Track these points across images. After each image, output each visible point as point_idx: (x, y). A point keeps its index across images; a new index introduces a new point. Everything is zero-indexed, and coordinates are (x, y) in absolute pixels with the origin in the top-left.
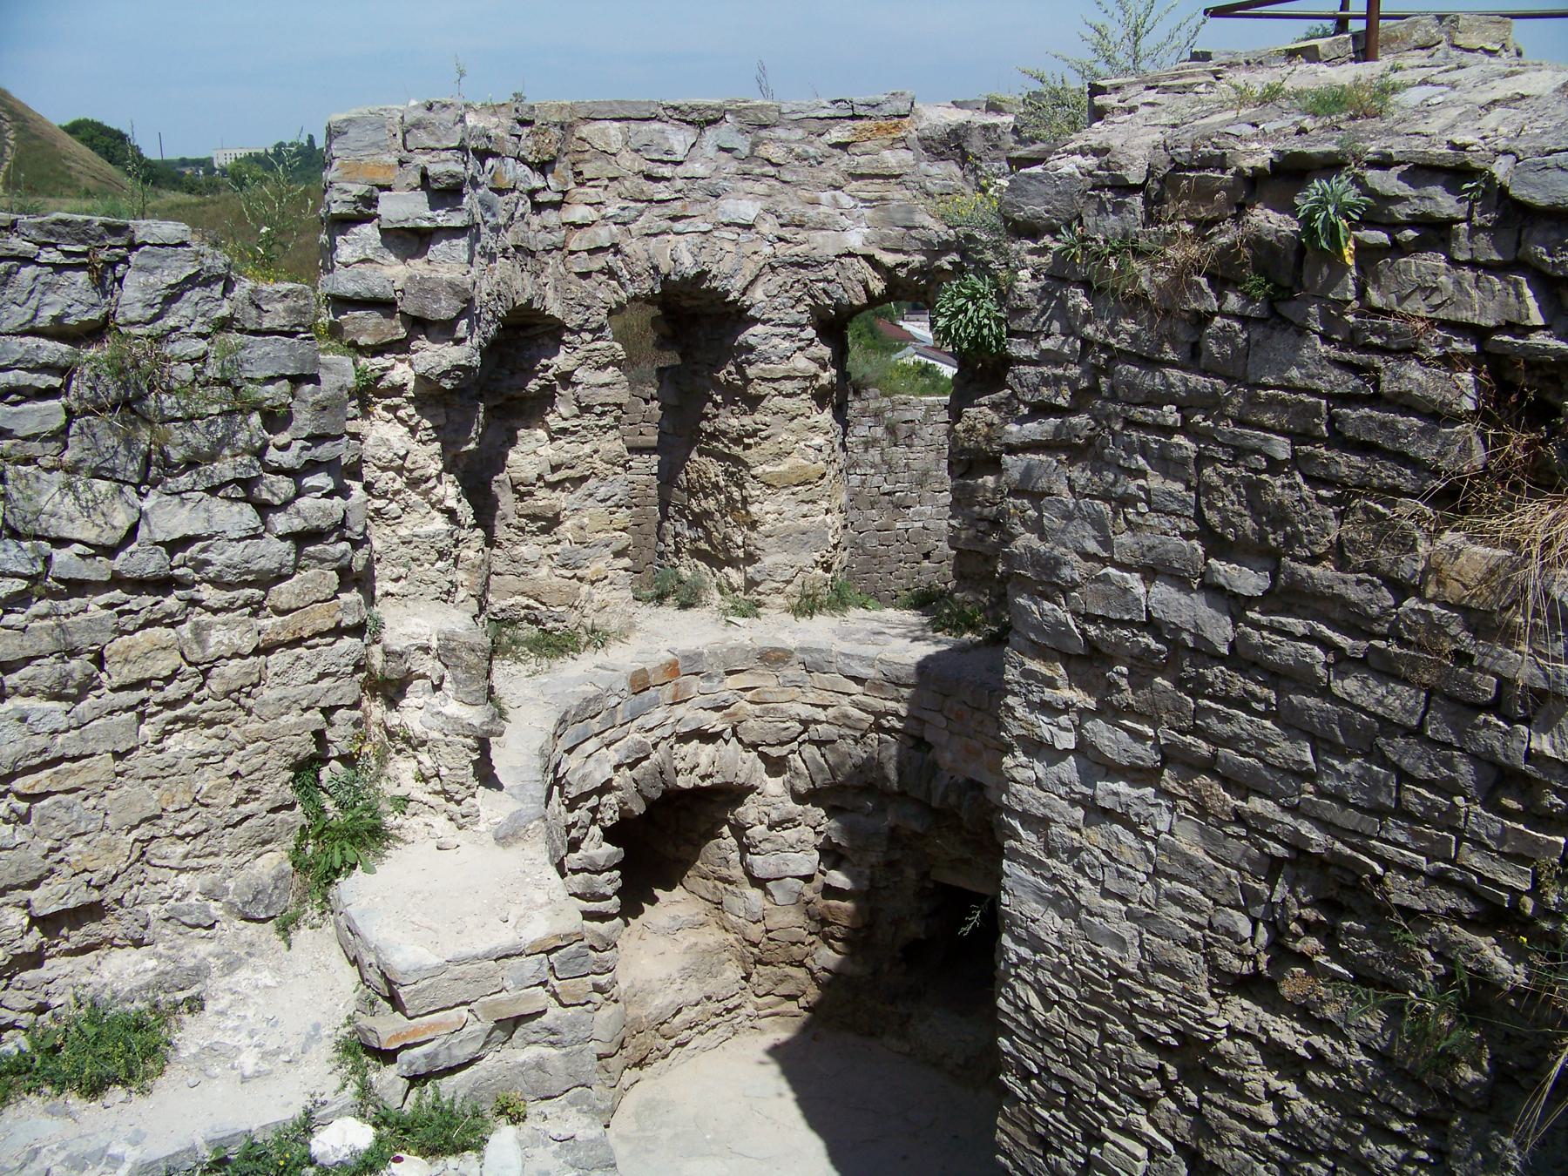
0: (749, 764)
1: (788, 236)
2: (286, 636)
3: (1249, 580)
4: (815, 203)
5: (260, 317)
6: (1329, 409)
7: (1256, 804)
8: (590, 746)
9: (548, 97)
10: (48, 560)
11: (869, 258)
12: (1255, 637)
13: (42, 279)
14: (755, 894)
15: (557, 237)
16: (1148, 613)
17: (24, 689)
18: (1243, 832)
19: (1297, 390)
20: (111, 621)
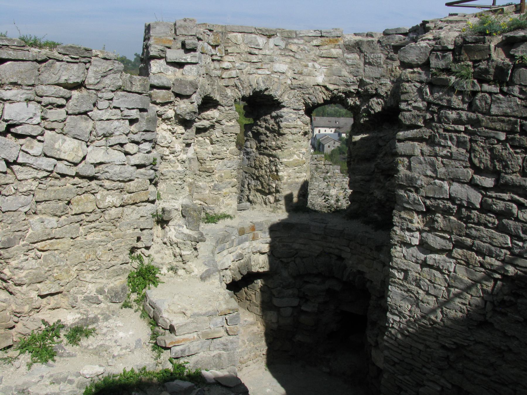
1: (297, 78)
2: (131, 202)
3: (488, 182)
5: (132, 86)
6: (520, 122)
9: (216, 22)
11: (325, 87)
12: (490, 201)
13: (63, 66)
15: (218, 73)
16: (450, 194)
17: (43, 212)
18: (483, 270)
19: (508, 116)
20: (74, 190)
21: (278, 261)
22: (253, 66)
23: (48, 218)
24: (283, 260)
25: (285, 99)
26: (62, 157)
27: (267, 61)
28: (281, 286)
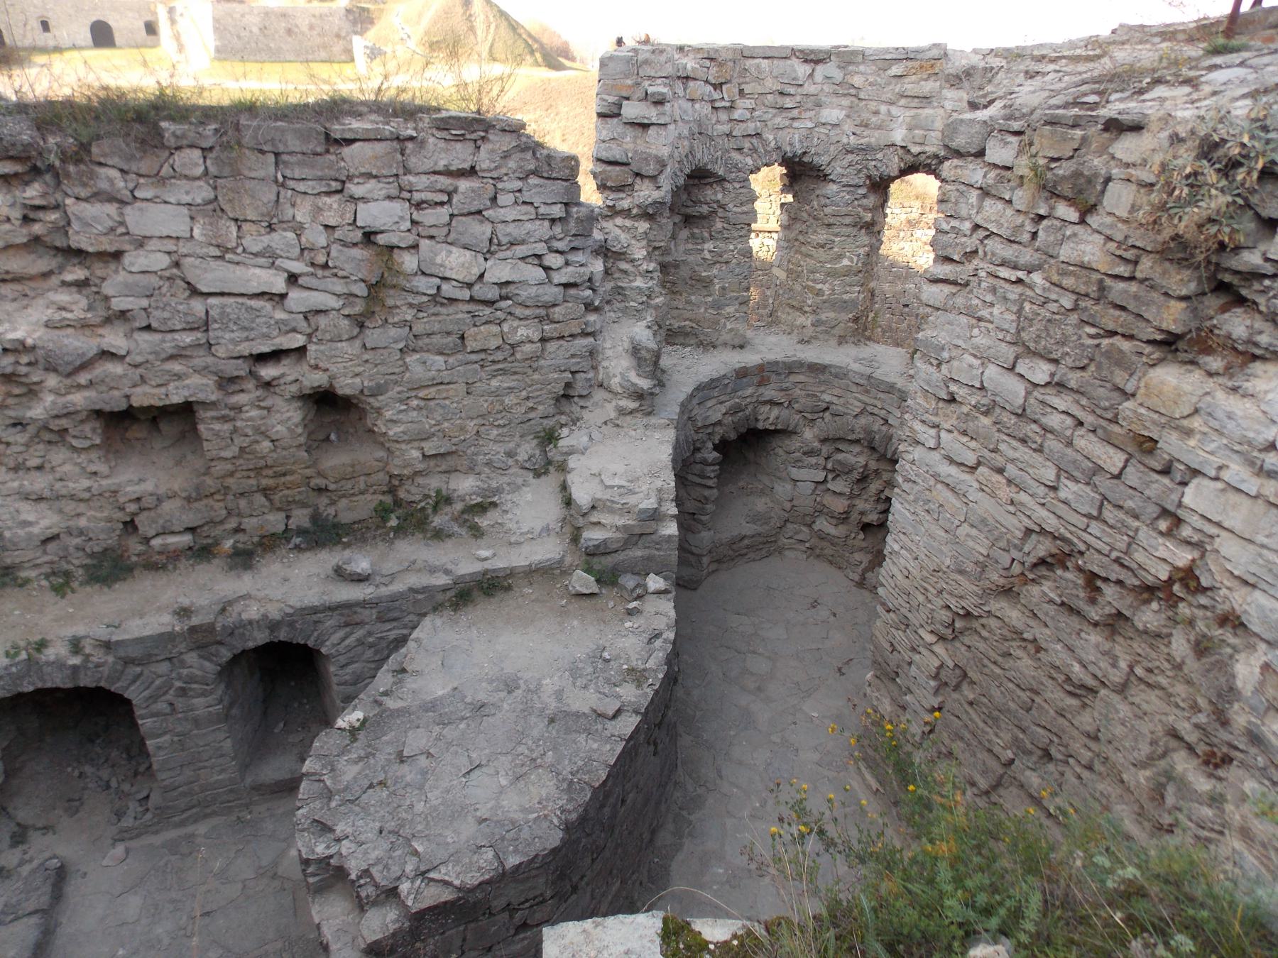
2: (555, 335)
4: (876, 113)
7: (1023, 497)
8: (709, 404)
10: (439, 288)
14: (789, 486)
15: (725, 128)
23: (432, 357)
25: (837, 170)
26: (448, 275)
27: (809, 105)
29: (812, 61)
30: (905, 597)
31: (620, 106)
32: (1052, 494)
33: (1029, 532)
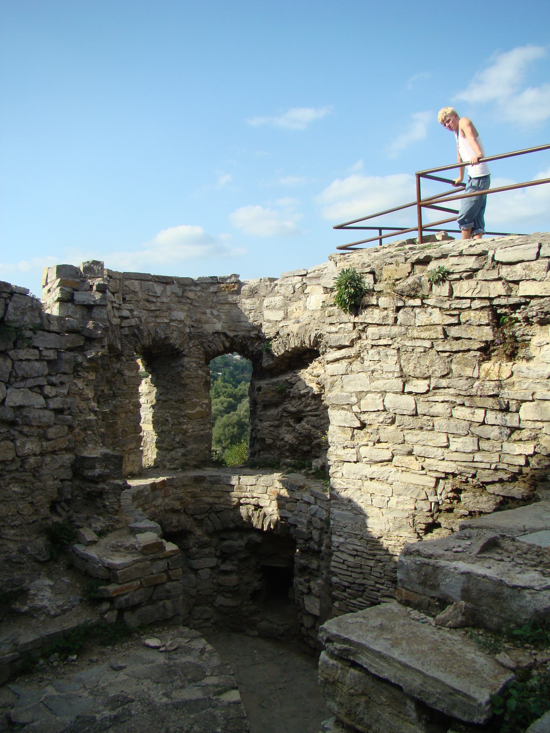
0: (190, 523)
5: (50, 325)
11: (225, 334)
21: (191, 519)
22: (151, 314)
24: (196, 517)
28: (197, 546)
29: (163, 283)
30: (359, 570)
31: (73, 295)
32: (446, 451)
33: (438, 479)
